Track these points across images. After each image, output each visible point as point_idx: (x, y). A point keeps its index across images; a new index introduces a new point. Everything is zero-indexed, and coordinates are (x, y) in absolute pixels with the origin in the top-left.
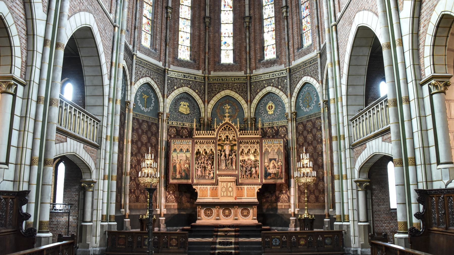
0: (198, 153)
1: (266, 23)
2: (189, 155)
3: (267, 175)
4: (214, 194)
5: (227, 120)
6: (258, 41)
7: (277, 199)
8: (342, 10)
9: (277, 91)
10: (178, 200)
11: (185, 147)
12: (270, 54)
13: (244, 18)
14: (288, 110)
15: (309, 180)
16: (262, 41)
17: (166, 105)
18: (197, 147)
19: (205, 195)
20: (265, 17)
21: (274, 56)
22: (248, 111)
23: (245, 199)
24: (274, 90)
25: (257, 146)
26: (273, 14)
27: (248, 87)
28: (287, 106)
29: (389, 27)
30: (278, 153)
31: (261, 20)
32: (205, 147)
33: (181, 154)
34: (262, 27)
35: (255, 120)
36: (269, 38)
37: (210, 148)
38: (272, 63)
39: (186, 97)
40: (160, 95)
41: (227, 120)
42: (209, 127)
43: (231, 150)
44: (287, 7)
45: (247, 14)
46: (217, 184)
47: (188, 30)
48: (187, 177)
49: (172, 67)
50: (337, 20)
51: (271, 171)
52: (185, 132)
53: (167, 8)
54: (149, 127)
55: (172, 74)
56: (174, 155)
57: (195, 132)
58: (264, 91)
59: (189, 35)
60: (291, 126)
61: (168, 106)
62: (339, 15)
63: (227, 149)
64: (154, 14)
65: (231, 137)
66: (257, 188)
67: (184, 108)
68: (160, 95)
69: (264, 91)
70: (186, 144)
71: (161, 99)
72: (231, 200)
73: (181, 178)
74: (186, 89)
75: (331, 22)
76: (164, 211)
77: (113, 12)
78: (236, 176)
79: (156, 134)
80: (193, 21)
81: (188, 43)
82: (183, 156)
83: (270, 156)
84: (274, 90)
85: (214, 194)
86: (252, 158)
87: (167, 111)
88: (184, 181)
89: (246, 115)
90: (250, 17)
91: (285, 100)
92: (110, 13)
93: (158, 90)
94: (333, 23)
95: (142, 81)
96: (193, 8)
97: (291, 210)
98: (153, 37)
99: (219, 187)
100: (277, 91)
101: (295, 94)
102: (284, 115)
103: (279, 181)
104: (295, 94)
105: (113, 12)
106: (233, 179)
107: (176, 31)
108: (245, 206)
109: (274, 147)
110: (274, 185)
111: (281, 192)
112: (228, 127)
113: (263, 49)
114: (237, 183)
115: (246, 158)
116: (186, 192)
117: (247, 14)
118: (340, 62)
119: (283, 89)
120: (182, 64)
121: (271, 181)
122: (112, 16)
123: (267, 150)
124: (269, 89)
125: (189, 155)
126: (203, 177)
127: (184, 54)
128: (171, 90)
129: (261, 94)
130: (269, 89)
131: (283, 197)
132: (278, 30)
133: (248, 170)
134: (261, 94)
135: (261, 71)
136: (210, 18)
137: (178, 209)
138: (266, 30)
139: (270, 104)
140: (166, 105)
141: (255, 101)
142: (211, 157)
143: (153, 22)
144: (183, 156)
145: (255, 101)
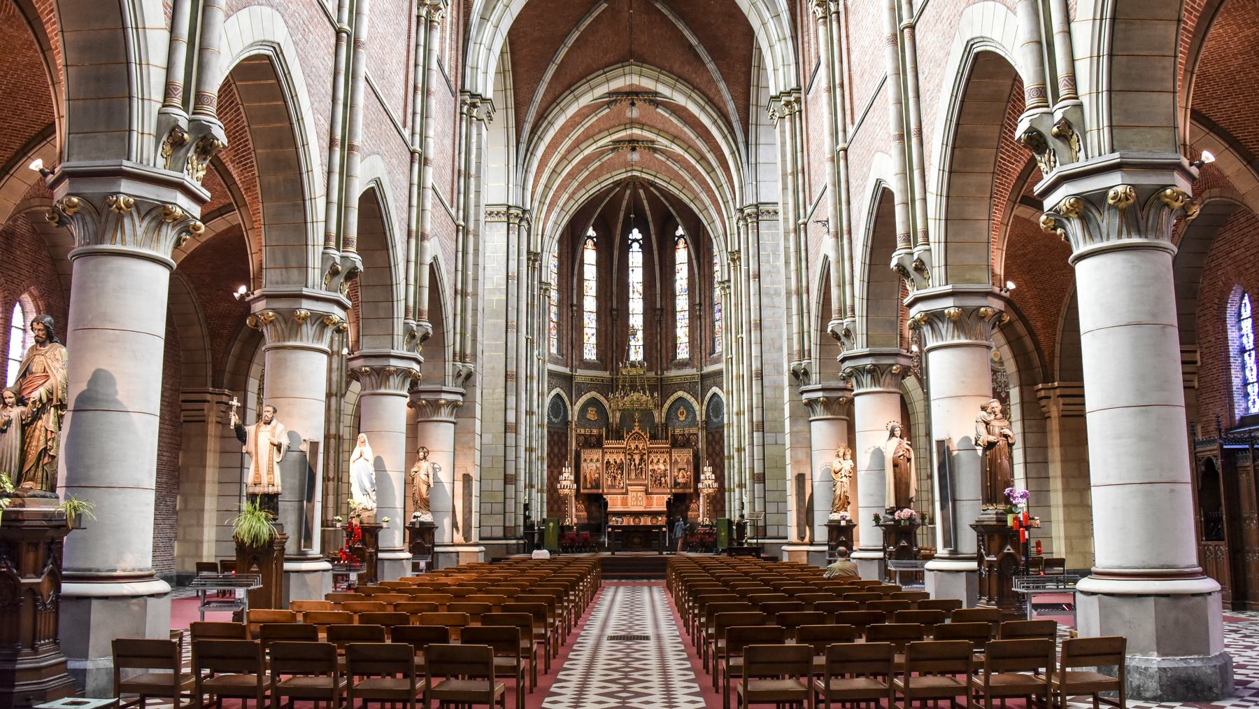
0: (608, 462)
1: (679, 316)
2: (599, 465)
3: (676, 484)
4: (624, 503)
5: (637, 429)
6: (670, 338)
7: (688, 509)
8: (857, 120)
9: (688, 397)
10: (588, 510)
11: (595, 457)
12: (683, 353)
13: (655, 310)
14: (698, 418)
15: (711, 491)
16: (675, 338)
17: (574, 412)
18: (607, 457)
19: (615, 503)
20: (678, 309)
21: (687, 356)
22: (659, 417)
23: (655, 508)
24: (685, 395)
25: (666, 456)
26: (686, 308)
27: (662, 388)
28: (698, 413)
29: (1043, 47)
30: (688, 462)
31: (674, 312)
32: (615, 456)
33: (592, 463)
34: (674, 321)
35: (665, 426)
36: (682, 333)
37: (619, 457)
38: (683, 364)
39: (593, 402)
40: (568, 403)
41: (637, 429)
42: (620, 437)
43: (641, 459)
44: (700, 304)
45: (658, 306)
46: (626, 493)
47: (594, 324)
48: (597, 487)
49: (580, 372)
50: (915, 13)
51: (680, 480)
52: (593, 440)
53: (572, 305)
54: (560, 437)
55: (578, 380)
56: (584, 465)
57: (605, 442)
58: (676, 396)
59: (594, 331)
60: (701, 435)
61: (576, 414)
62: (850, 135)
63: (637, 458)
64: (559, 315)
65: (641, 447)
66: (666, 498)
67: (591, 415)
68: (568, 403)
69: (676, 396)
70: (596, 454)
71: (569, 408)
72: (641, 509)
73: (592, 488)
74: (593, 394)
75: (901, 20)
76: (575, 520)
77: (409, 123)
78: (646, 485)
79: (566, 444)
80: (599, 313)
81: (593, 340)
82: (593, 466)
83: (680, 466)
84: (685, 395)
85: (624, 503)
86: (662, 467)
87: (576, 418)
88: (595, 491)
89: (656, 420)
90: (662, 309)
91: (697, 407)
92: (405, 126)
93: (566, 399)
94: (906, 21)
95: (553, 393)
96: (598, 297)
97: (700, 519)
98: (559, 341)
99: (629, 496)
100: (688, 397)
101: (705, 403)
102: (694, 423)
103: (688, 491)
104: (705, 403)
105: (409, 123)
106: (642, 488)
107: (580, 328)
108: (654, 514)
109: (683, 456)
110: (684, 495)
111: (691, 501)
112: (638, 437)
113: (675, 346)
114: (647, 492)
115: (656, 467)
116: (595, 501)
117: (658, 306)
118: (924, 130)
119: (695, 396)
120: (588, 365)
121: (680, 491)
122: (407, 133)
123: (676, 461)
124: (680, 393)
125: (599, 465)
126: (613, 487)
127: (590, 354)
128: (579, 396)
129: (672, 398)
130: (680, 393)
131: (693, 506)
132: (691, 327)
133: (658, 480)
134: (672, 398)
135: (673, 373)
136: (617, 310)
137: (588, 518)
138: (679, 325)
139: (682, 409)
140: (574, 412)
141: (666, 406)
142: (620, 467)
143: (558, 324)
144: (593, 466)
145: (666, 406)
